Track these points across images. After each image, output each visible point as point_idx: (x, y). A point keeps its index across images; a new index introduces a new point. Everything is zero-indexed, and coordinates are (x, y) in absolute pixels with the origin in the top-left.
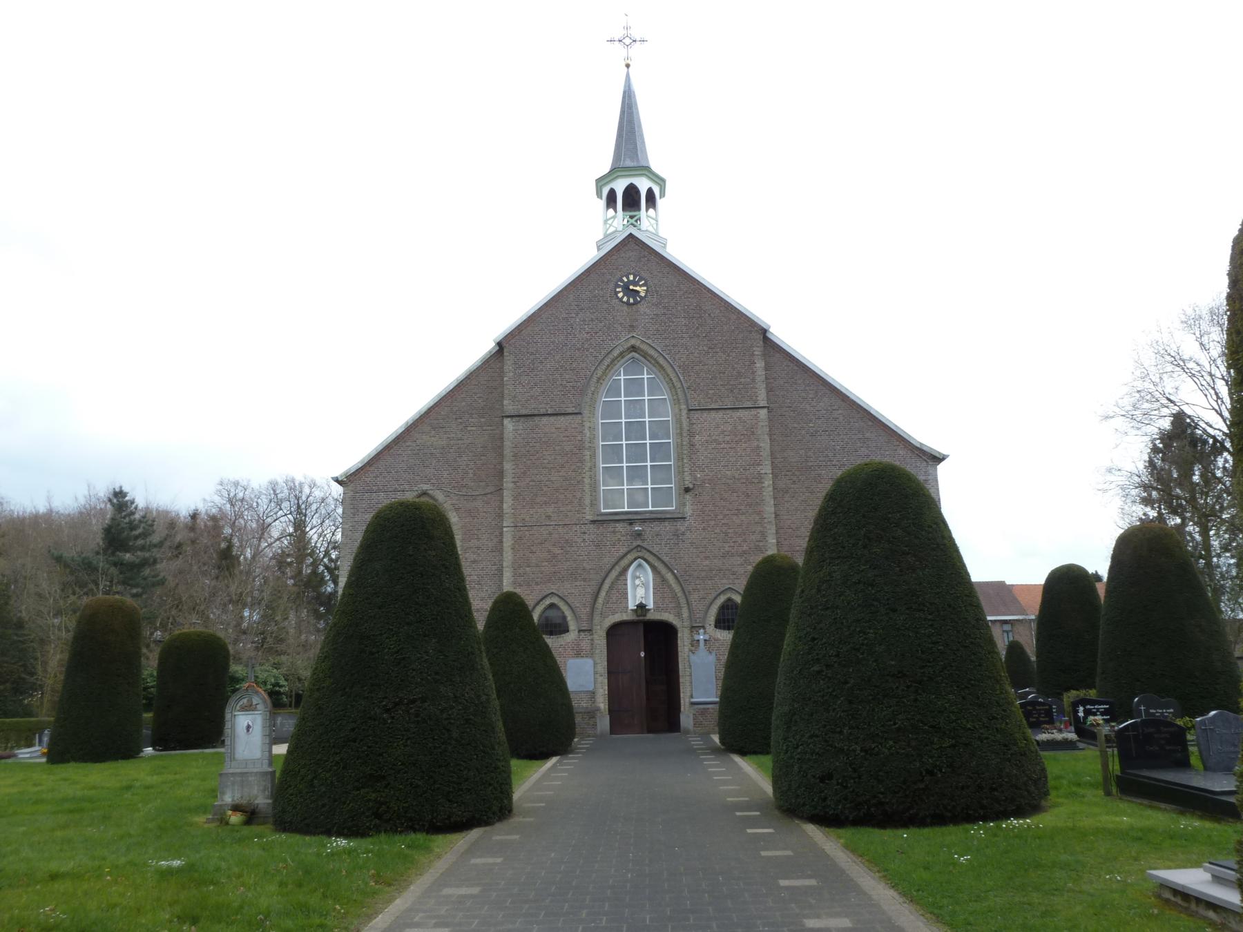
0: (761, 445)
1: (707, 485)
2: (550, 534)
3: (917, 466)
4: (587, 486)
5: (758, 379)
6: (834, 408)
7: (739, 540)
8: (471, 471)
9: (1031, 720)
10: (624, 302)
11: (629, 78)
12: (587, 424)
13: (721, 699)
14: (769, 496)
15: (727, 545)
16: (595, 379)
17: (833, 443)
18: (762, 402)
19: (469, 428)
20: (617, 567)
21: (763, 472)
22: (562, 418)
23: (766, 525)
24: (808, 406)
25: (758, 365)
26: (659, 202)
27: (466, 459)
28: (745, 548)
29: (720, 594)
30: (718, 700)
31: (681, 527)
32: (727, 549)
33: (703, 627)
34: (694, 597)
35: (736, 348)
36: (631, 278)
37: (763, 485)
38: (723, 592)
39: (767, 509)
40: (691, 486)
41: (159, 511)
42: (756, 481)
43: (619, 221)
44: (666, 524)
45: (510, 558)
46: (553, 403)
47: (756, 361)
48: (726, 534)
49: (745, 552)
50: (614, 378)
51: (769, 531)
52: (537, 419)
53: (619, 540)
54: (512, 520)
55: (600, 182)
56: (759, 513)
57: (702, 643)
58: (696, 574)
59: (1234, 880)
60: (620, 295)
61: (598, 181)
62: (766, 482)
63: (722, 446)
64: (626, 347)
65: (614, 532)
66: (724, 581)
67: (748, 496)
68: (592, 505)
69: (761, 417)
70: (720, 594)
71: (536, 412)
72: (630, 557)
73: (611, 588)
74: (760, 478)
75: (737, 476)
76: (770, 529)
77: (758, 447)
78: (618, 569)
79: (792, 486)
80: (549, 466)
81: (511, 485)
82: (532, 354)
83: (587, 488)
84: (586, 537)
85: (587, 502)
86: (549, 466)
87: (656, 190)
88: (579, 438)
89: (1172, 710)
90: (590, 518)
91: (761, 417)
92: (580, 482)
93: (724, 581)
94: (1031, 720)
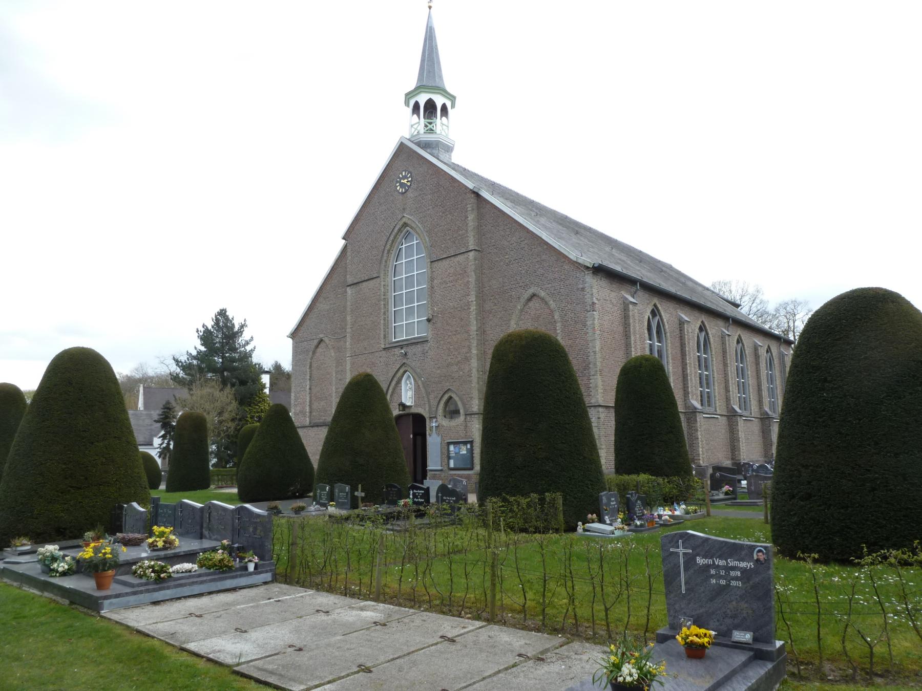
3: (577, 277)
5: (470, 229)
6: (522, 239)
9: (415, 500)
10: (400, 193)
12: (383, 283)
22: (371, 282)
25: (469, 218)
28: (459, 359)
30: (614, 405)
31: (426, 347)
32: (449, 360)
33: (435, 417)
35: (457, 209)
36: (404, 174)
39: (472, 328)
41: (247, 358)
42: (466, 308)
43: (419, 123)
44: (419, 346)
48: (449, 349)
49: (459, 362)
52: (360, 284)
55: (409, 96)
56: (467, 332)
57: (434, 428)
59: (106, 602)
60: (398, 188)
61: (407, 95)
63: (448, 285)
65: (394, 355)
66: (447, 384)
67: (462, 320)
68: (385, 337)
69: (471, 258)
72: (401, 371)
73: (393, 392)
74: (468, 304)
75: (456, 306)
77: (468, 282)
78: (396, 379)
79: (494, 307)
80: (366, 315)
82: (359, 242)
84: (381, 359)
85: (382, 336)
86: (366, 315)
89: (454, 499)
90: (383, 346)
91: (471, 258)
92: (379, 323)
94: (415, 500)
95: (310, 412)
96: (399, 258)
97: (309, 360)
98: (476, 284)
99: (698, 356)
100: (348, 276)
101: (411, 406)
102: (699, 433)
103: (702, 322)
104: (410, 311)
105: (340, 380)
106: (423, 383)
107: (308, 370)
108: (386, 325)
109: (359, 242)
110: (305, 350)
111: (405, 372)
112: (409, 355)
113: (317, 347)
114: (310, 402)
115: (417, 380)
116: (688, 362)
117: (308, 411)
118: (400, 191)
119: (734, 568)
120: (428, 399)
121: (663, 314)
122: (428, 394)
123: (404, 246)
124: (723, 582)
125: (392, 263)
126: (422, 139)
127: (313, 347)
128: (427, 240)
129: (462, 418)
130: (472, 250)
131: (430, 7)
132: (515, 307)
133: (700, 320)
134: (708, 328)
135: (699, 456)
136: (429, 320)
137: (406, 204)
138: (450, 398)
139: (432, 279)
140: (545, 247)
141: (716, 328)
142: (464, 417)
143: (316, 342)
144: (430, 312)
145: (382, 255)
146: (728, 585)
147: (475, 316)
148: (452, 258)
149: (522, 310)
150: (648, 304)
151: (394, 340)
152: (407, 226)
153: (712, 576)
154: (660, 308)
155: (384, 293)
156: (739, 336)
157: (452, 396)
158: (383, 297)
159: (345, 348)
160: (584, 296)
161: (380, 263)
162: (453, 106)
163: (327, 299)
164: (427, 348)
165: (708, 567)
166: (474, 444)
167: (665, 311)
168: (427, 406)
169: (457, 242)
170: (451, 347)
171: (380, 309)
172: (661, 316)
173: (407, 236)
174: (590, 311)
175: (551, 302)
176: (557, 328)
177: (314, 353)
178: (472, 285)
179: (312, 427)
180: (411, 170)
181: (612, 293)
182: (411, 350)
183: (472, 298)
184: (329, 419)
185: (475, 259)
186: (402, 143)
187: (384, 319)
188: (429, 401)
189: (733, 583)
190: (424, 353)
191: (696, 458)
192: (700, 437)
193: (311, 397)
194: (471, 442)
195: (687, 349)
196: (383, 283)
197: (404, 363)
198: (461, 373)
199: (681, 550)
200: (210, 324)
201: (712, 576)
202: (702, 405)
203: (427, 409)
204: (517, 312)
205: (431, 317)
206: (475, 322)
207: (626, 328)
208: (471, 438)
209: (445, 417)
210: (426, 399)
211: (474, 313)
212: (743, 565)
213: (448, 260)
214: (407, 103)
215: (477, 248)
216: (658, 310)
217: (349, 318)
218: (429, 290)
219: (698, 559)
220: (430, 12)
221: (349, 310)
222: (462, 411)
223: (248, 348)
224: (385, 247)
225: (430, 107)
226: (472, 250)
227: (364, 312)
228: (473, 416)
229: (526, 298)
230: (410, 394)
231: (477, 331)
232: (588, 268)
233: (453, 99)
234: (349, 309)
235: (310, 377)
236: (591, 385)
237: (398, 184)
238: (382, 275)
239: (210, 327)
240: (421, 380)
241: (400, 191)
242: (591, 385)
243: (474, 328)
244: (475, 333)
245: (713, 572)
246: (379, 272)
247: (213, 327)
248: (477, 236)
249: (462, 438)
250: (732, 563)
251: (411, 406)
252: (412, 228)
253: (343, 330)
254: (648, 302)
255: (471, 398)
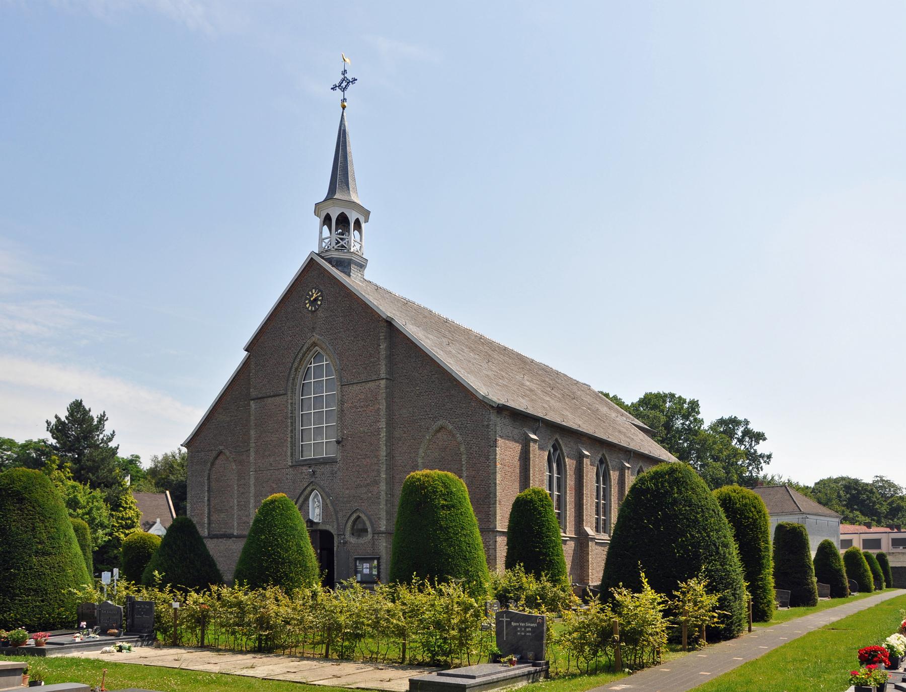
0: (381, 407)
1: (350, 438)
2: (271, 475)
3: (482, 414)
4: (289, 443)
6: (432, 373)
7: (365, 476)
8: (241, 436)
10: (309, 311)
11: (344, 131)
12: (290, 401)
13: (508, 529)
14: (383, 444)
15: (358, 480)
16: (293, 370)
17: (430, 401)
18: (383, 375)
19: (240, 408)
20: (302, 496)
21: (380, 427)
22: (277, 398)
23: (380, 465)
24: (417, 374)
25: (381, 347)
26: (363, 225)
27: (238, 428)
29: (352, 513)
30: (506, 530)
34: (340, 514)
35: (370, 335)
37: (380, 436)
38: (355, 512)
39: (382, 453)
40: (341, 439)
45: (253, 491)
46: (274, 388)
47: (381, 344)
48: (358, 472)
49: (368, 484)
50: (309, 366)
51: (382, 469)
53: (304, 478)
54: (254, 467)
56: (377, 457)
58: (341, 499)
60: (308, 305)
62: (382, 434)
64: (310, 344)
65: (302, 473)
66: (356, 504)
68: (292, 455)
70: (352, 513)
71: (265, 395)
72: (309, 489)
74: (378, 430)
76: (383, 468)
80: (271, 431)
81: (254, 445)
83: (289, 445)
85: (289, 454)
87: (362, 220)
88: (285, 411)
93: (356, 504)
95: (209, 524)
96: (307, 377)
97: (207, 472)
98: (386, 411)
99: (597, 486)
100: (251, 390)
101: (318, 524)
102: (590, 556)
103: (603, 455)
104: (318, 431)
105: (242, 493)
106: (332, 502)
107: (206, 482)
108: (293, 444)
109: (264, 355)
110: (202, 460)
111: (313, 490)
112: (318, 474)
113: (216, 458)
114: (209, 513)
115: (325, 498)
116: (585, 492)
117: (206, 522)
118: (310, 309)
119: (528, 627)
120: (336, 516)
121: (563, 448)
122: (336, 512)
123: (313, 365)
124: (523, 634)
125: (299, 381)
126: (333, 256)
127: (211, 459)
128: (338, 362)
129: (370, 536)
130: (383, 379)
131: (344, 107)
132: (424, 436)
133: (601, 453)
134: (608, 460)
135: (589, 577)
136: (338, 442)
137: (316, 323)
138: (359, 517)
139: (342, 402)
140: (455, 383)
141: (617, 460)
142: (372, 535)
143: (214, 453)
144: (339, 434)
145: (290, 372)
146: (525, 635)
147: (385, 442)
148: (363, 384)
149: (430, 440)
150: (549, 439)
151: (301, 458)
152: (317, 346)
153: (518, 631)
154: (561, 443)
155: (292, 411)
156: (641, 467)
157: (361, 515)
158: (290, 415)
159: (249, 462)
160: (488, 432)
161: (288, 380)
162: (366, 221)
163: (228, 411)
164: (336, 469)
165: (516, 627)
166: (381, 561)
167: (566, 445)
168: (335, 523)
169: (368, 368)
170: (360, 470)
171: (287, 427)
172: (561, 450)
173: (317, 358)
174: (493, 447)
175: (458, 435)
176: (463, 460)
177: (213, 464)
178: (383, 412)
179: (211, 538)
180: (321, 287)
181: (516, 430)
182: (320, 470)
183: (383, 425)
184: (246, 533)
185: (386, 388)
186: (312, 258)
187: (292, 437)
188: (337, 519)
189: (528, 634)
190: (333, 473)
191: (585, 578)
192: (590, 560)
193: (209, 509)
194: (378, 559)
195: (585, 481)
196: (290, 401)
197: (312, 482)
198: (370, 494)
199: (505, 619)
200: (63, 415)
201: (518, 631)
202: (597, 531)
203: (335, 527)
204: (426, 441)
205: (341, 439)
206: (385, 448)
207: (526, 462)
208: (379, 555)
209: (353, 534)
210: (334, 517)
211: (384, 439)
212: (532, 625)
213: (359, 385)
214: (317, 213)
215: (388, 377)
216: (559, 445)
217: (252, 432)
218: (339, 413)
219: (512, 623)
220: (343, 111)
221: (254, 425)
222: (369, 530)
223: (112, 444)
224: (292, 364)
225: (343, 221)
226: (383, 379)
227: (269, 428)
228: (380, 535)
229: (434, 429)
230: (317, 511)
231: (386, 457)
232: (493, 407)
233: (367, 214)
234: (252, 424)
235: (209, 488)
236: (490, 513)
237: (307, 302)
238: (289, 393)
239: (63, 419)
240: (330, 499)
241: (310, 309)
242: (490, 513)
243: (383, 453)
244: (385, 458)
245: (519, 629)
246: (286, 390)
247: (67, 418)
248: (389, 365)
249: (370, 555)
250: (528, 624)
251: (320, 523)
252: (321, 348)
253: (246, 444)
254: (550, 437)
255: (379, 518)
